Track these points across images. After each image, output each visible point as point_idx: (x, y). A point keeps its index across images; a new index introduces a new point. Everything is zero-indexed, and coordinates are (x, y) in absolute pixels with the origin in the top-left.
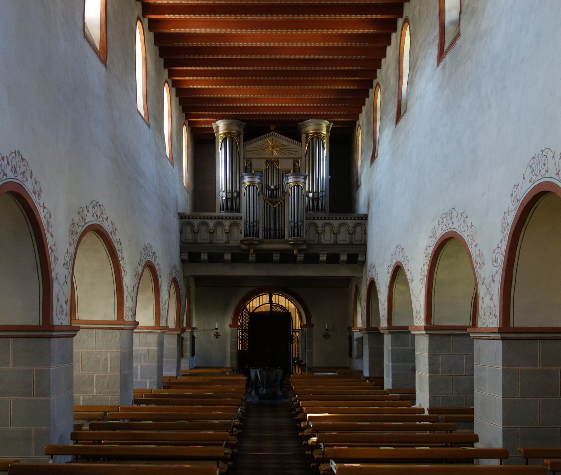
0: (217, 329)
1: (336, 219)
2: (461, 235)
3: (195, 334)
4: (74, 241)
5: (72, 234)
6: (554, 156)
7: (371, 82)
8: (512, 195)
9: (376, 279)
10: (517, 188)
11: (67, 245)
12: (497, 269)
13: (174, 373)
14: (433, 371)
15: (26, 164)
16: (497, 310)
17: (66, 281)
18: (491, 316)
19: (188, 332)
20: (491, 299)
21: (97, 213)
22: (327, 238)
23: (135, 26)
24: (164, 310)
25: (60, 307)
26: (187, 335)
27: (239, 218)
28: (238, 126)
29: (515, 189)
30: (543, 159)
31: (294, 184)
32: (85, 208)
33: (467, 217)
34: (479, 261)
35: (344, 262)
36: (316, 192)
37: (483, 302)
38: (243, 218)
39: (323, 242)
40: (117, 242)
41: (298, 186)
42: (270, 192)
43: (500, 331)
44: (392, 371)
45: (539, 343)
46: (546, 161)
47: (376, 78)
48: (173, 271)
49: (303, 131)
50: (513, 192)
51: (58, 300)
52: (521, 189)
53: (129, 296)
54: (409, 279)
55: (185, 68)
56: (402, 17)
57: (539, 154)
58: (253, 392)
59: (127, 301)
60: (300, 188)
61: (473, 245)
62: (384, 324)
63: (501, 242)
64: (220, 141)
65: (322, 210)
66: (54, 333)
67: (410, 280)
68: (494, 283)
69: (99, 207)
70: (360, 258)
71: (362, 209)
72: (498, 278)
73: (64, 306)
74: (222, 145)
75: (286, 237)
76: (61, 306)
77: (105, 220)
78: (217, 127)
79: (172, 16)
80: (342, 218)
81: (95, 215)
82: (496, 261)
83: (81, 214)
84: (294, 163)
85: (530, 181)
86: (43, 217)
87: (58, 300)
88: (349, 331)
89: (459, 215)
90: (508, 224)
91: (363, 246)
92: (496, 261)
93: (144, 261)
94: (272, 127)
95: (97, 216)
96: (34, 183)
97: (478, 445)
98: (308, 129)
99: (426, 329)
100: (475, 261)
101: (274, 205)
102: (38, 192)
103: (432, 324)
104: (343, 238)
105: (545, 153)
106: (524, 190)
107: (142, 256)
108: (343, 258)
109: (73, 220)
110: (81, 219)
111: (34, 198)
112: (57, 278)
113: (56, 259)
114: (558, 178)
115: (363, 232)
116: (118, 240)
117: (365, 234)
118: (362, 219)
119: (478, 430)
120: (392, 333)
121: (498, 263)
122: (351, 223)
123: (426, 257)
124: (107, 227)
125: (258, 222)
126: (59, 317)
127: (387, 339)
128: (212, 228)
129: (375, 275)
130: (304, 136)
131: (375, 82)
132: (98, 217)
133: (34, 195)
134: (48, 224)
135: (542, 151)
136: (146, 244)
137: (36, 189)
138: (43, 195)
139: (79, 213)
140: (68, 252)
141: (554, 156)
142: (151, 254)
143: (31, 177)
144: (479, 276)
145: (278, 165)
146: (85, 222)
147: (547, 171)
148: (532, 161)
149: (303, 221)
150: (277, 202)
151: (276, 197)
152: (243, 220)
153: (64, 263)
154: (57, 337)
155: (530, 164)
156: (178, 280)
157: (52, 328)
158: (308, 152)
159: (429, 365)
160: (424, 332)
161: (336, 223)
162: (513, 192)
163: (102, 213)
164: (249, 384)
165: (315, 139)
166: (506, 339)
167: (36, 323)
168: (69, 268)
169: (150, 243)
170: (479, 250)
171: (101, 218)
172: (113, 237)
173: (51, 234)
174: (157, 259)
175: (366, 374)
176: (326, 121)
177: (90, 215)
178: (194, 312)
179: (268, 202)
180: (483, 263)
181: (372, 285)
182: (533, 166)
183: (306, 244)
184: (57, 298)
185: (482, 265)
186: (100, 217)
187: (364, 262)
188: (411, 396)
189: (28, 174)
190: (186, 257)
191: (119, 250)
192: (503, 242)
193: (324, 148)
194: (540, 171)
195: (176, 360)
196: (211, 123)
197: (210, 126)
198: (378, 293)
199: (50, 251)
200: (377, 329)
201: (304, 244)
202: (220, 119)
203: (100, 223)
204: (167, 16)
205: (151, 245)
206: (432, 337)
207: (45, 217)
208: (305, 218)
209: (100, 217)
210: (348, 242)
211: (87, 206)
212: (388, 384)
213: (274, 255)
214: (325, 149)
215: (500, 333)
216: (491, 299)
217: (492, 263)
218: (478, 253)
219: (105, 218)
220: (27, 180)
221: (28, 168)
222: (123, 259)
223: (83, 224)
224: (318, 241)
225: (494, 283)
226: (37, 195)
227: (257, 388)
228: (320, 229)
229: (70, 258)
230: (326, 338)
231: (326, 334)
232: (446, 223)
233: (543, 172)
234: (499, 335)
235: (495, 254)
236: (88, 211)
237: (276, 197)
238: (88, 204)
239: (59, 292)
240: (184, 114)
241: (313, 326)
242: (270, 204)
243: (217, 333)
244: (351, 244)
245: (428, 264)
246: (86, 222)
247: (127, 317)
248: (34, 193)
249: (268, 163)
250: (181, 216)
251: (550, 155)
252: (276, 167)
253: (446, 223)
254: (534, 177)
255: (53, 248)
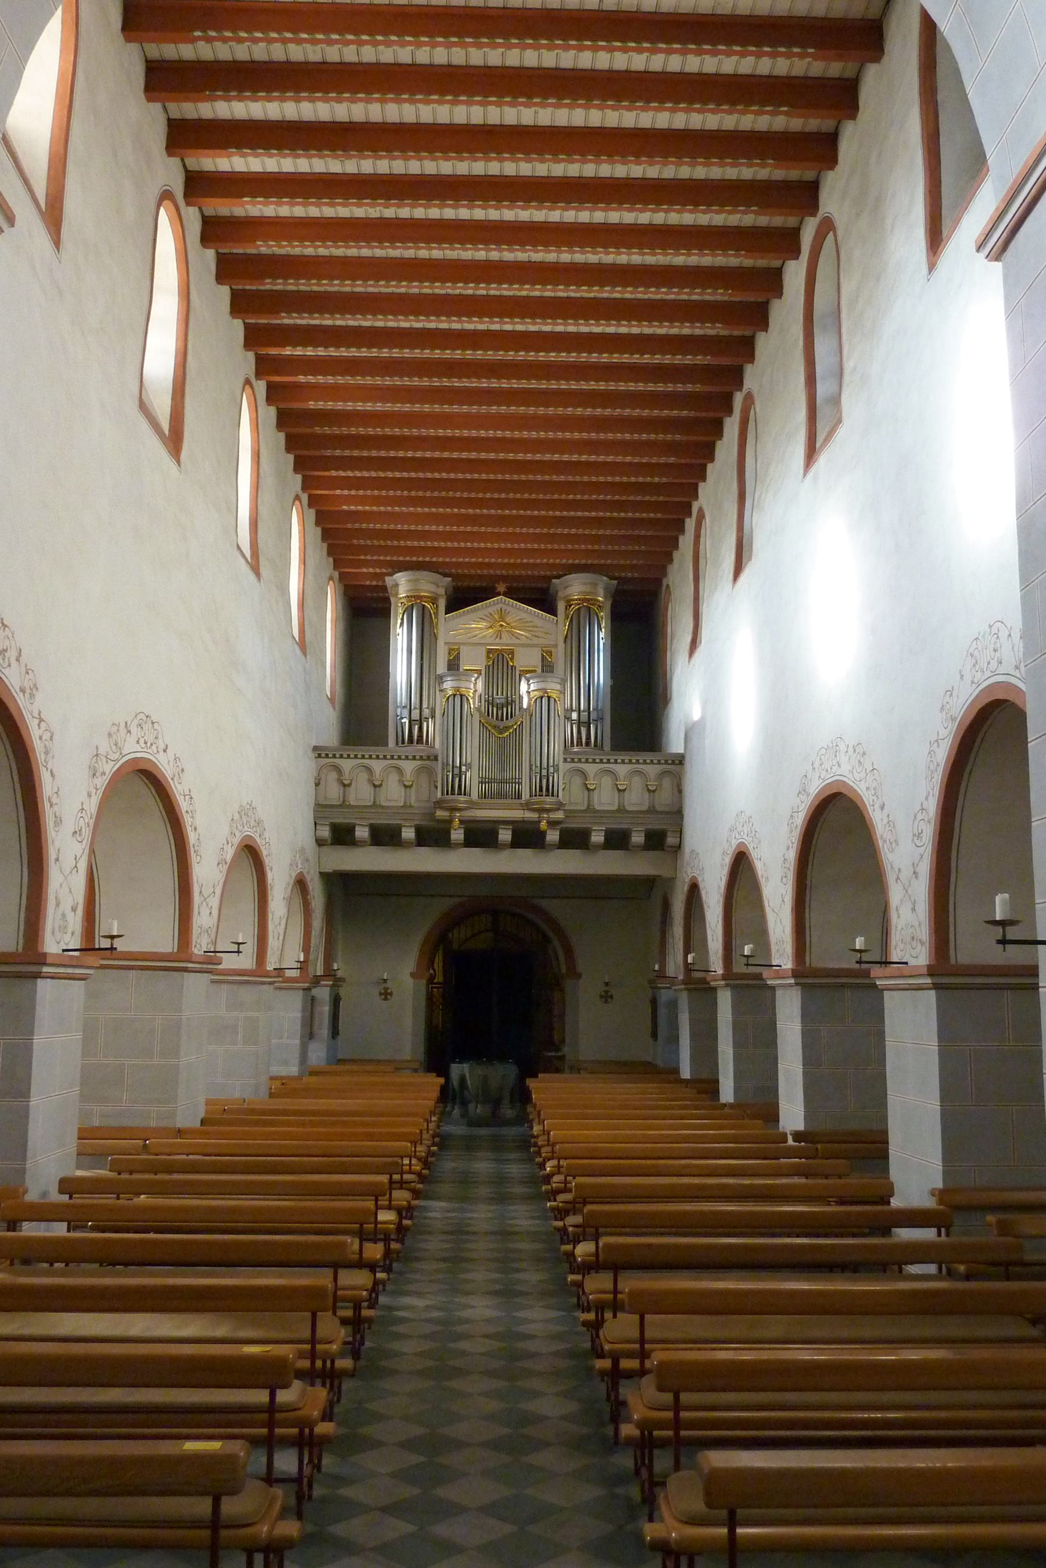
0: (385, 981)
1: (623, 762)
2: (855, 787)
3: (342, 992)
4: (97, 789)
5: (94, 774)
6: (1010, 635)
7: (689, 506)
8: (942, 709)
9: (700, 879)
10: (951, 695)
11: (84, 797)
12: (923, 848)
13: (293, 1070)
14: (810, 1060)
15: (10, 636)
16: (924, 932)
17: (76, 867)
18: (914, 944)
19: (326, 986)
20: (913, 909)
21: (146, 738)
22: (605, 799)
23: (240, 397)
24: (276, 937)
25: (60, 917)
26: (323, 993)
27: (432, 758)
28: (431, 583)
29: (947, 699)
30: (993, 640)
31: (541, 694)
32: (123, 725)
33: (864, 754)
34: (887, 836)
35: (638, 847)
36: (584, 711)
37: (899, 917)
38: (440, 758)
39: (597, 807)
40: (185, 796)
41: (549, 697)
42: (495, 709)
43: (931, 971)
44: (735, 1065)
45: (1007, 995)
46: (998, 645)
47: (696, 497)
48: (298, 858)
49: (560, 594)
50: (945, 703)
51: (58, 905)
52: (958, 696)
53: (204, 903)
54: (762, 877)
55: (334, 473)
56: (741, 390)
57: (985, 633)
58: (455, 1111)
59: (199, 913)
60: (552, 701)
61: (877, 806)
62: (717, 966)
63: (927, 798)
64: (400, 611)
65: (596, 745)
66: (45, 969)
67: (764, 879)
68: (916, 877)
69: (151, 725)
70: (671, 840)
71: (675, 744)
72: (925, 868)
73: (70, 915)
74: (402, 619)
75: (525, 795)
76: (64, 915)
77: (162, 752)
78: (397, 585)
79: (311, 379)
80: (634, 761)
81: (142, 741)
82: (919, 836)
83: (114, 737)
84: (542, 655)
85: (973, 682)
86: (38, 739)
87: (58, 905)
88: (652, 988)
89: (851, 750)
90: (938, 765)
91: (677, 814)
92: (919, 836)
93: (238, 836)
94: (501, 587)
95: (146, 743)
96: (23, 670)
97: (896, 1203)
98: (569, 591)
99: (796, 974)
100: (882, 837)
101: (501, 733)
102: (31, 690)
103: (807, 965)
104: (636, 799)
105: (994, 630)
106: (962, 701)
107: (234, 826)
108: (637, 838)
109: (97, 748)
110: (114, 747)
111: (21, 700)
112: (57, 860)
113: (58, 821)
114: (1018, 675)
115: (676, 789)
116: (187, 793)
117: (680, 791)
118: (673, 763)
119: (895, 1173)
120: (733, 988)
121: (924, 839)
122: (652, 770)
123: (791, 832)
124: (166, 767)
125: (469, 766)
126: (58, 935)
127: (725, 1000)
128: (378, 776)
129: (698, 872)
130: (561, 606)
131: (738, 399)
132: (149, 745)
133: (21, 695)
134: (47, 753)
135: (990, 626)
136: (244, 803)
137: (27, 684)
138: (39, 696)
139: (110, 735)
140: (83, 809)
141: (1010, 635)
142: (253, 823)
143: (18, 660)
144: (889, 866)
145: (512, 659)
146: (121, 754)
147: (1001, 663)
148: (974, 646)
149: (558, 765)
150: (507, 728)
151: (507, 719)
152: (440, 762)
153: (73, 830)
154: (52, 978)
155: (971, 650)
156: (308, 878)
157: (42, 959)
158: (569, 634)
159: (803, 1048)
160: (792, 981)
161: (622, 770)
162: (945, 703)
163: (156, 738)
164: (446, 1095)
165: (582, 612)
166: (942, 988)
167: (12, 949)
168: (85, 842)
169: (252, 802)
170: (888, 816)
171: (154, 747)
172: (176, 784)
173: (51, 772)
174: (266, 835)
175: (686, 1073)
176: (605, 578)
177: (131, 740)
178: (340, 953)
179: (489, 728)
180: (895, 841)
181: (694, 889)
182: (976, 653)
183: (564, 810)
184: (56, 898)
185: (894, 845)
186: (152, 745)
187: (679, 847)
188: (771, 1115)
189: (12, 654)
190: (325, 832)
191: (187, 812)
192: (930, 798)
193: (600, 629)
194: (989, 663)
195: (298, 1042)
196: (381, 576)
197: (380, 583)
198: (705, 906)
199: (47, 805)
200: (704, 981)
201: (558, 809)
202: (400, 571)
203: (151, 757)
204: (301, 379)
205: (254, 805)
206: (807, 989)
207: (41, 738)
208: (562, 760)
209: (152, 745)
210: (645, 808)
211: (126, 723)
212: (727, 1093)
213: (500, 831)
214: (603, 630)
215: (930, 974)
216: (913, 909)
217: (913, 840)
218: (885, 821)
219: (162, 746)
220: (9, 666)
221: (13, 643)
222: (195, 829)
223: (116, 756)
224: (589, 805)
225: (916, 877)
226: (27, 695)
227: (464, 1104)
228: (591, 783)
229: (87, 821)
230: (606, 1002)
231: (606, 992)
232: (827, 766)
233: (994, 664)
234: (929, 980)
235: (916, 823)
236: (129, 732)
237: (507, 719)
238: (129, 720)
239: (61, 886)
240: (331, 560)
241: (579, 976)
242: (493, 731)
243: (386, 989)
244: (652, 810)
245: (795, 845)
246: (124, 752)
247: (198, 946)
248: (23, 691)
249: (491, 655)
250: (319, 752)
251: (1004, 634)
252: (508, 662)
253: (827, 766)
254: (979, 674)
255: (54, 800)
